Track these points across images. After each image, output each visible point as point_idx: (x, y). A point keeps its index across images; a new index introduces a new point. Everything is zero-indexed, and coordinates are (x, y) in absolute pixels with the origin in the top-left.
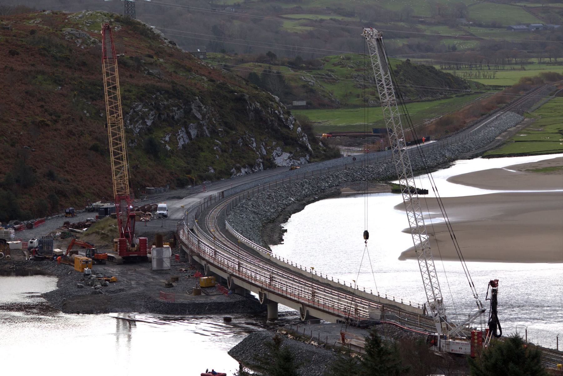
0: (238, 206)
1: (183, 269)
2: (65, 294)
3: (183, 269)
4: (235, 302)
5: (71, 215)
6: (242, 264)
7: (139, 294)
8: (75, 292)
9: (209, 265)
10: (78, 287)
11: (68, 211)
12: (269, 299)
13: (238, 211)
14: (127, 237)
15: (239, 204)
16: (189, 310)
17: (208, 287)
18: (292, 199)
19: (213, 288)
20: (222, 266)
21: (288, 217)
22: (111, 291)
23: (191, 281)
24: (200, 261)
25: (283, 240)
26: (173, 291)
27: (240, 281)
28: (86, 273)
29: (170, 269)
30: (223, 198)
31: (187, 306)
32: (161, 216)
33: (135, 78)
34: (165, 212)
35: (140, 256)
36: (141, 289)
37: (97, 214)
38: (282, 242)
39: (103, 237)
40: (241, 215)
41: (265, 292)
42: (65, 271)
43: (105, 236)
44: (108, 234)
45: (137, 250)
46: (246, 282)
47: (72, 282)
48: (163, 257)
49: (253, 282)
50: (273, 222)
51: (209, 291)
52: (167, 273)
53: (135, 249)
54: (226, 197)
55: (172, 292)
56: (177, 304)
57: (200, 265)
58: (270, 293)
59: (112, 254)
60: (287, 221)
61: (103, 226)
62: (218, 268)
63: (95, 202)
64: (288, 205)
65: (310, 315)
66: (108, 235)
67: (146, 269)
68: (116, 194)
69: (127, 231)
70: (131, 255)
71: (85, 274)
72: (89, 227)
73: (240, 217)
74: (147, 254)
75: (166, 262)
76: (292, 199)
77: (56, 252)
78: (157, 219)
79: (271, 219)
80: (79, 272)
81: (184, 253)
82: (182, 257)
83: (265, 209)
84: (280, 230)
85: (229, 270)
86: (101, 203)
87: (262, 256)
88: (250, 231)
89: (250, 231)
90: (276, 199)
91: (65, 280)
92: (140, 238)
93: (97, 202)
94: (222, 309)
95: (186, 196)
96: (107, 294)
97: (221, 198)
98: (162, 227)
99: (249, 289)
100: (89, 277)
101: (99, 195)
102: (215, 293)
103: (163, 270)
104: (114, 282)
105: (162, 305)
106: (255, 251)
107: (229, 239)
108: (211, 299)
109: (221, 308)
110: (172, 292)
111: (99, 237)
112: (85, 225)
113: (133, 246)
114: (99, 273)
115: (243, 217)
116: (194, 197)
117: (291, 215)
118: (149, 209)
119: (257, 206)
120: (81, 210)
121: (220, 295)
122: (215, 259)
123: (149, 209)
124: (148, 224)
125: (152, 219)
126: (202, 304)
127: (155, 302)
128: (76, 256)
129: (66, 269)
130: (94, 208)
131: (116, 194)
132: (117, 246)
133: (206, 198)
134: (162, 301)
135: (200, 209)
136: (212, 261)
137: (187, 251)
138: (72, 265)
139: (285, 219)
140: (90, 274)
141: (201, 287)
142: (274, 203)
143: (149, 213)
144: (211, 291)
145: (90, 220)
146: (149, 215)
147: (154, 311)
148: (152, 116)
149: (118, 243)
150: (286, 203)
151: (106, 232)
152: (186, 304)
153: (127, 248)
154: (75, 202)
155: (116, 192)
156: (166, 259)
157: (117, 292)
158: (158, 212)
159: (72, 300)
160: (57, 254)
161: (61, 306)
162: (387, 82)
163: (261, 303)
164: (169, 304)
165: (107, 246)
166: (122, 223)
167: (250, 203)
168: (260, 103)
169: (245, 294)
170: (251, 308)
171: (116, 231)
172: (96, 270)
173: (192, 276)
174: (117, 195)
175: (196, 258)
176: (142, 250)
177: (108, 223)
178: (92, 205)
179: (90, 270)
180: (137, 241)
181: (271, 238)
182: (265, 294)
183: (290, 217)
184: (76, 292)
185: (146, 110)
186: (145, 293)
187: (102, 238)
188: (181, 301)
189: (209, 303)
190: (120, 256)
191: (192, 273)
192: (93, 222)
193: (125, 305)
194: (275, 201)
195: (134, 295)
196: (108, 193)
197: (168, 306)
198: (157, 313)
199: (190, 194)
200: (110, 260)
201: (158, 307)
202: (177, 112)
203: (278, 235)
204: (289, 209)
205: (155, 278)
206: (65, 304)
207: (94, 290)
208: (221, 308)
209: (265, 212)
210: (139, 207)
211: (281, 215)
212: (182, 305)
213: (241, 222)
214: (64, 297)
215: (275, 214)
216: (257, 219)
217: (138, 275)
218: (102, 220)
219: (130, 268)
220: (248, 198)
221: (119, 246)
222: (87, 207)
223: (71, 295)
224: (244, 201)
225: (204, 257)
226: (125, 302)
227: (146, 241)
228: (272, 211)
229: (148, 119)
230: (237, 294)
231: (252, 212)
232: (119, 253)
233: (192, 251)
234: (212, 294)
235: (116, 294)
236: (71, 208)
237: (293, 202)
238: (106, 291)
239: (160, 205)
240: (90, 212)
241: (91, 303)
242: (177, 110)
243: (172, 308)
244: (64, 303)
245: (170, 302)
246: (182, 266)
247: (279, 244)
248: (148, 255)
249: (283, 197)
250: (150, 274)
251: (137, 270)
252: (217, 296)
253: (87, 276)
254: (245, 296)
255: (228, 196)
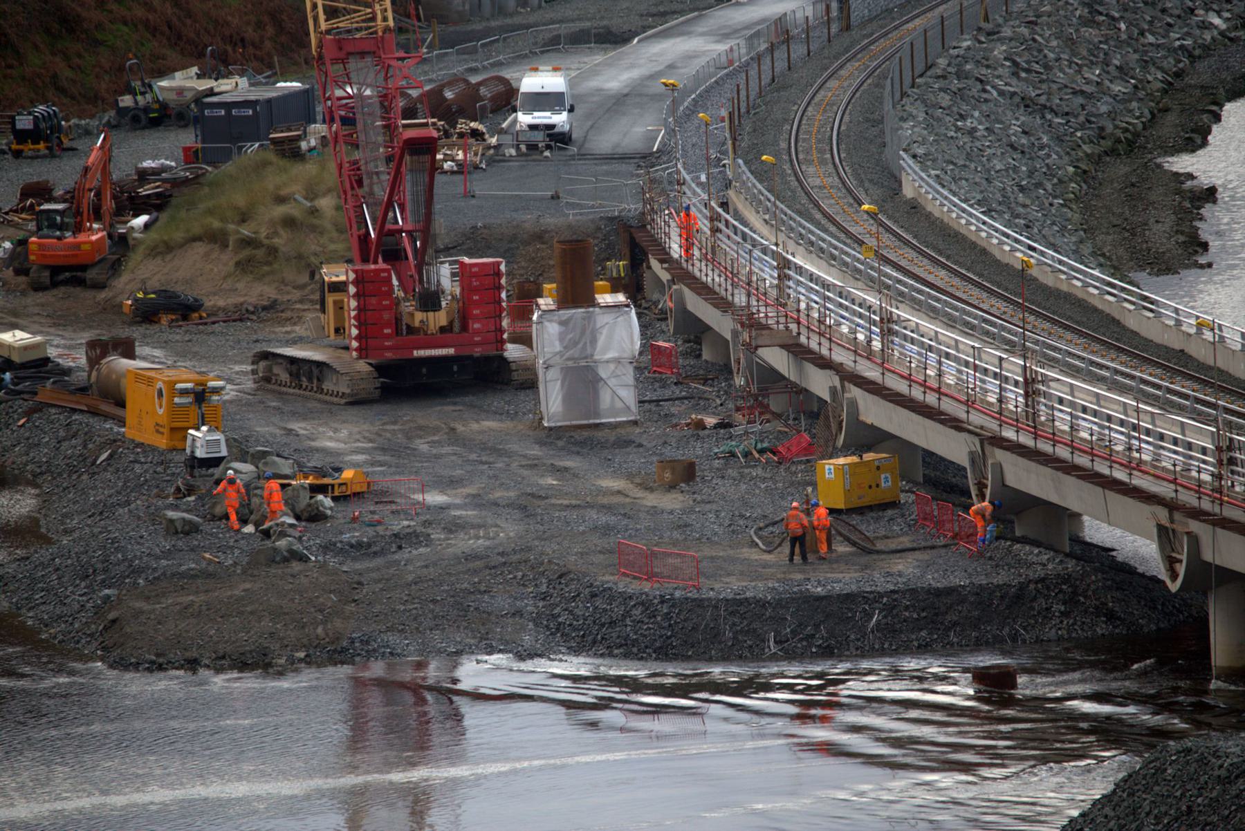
0: (939, 72)
1: (711, 421)
2: (105, 570)
3: (711, 421)
4: (1022, 587)
5: (42, 145)
6: (1045, 380)
7: (502, 554)
8: (158, 558)
9: (855, 392)
10: (172, 529)
11: (24, 122)
12: (1218, 562)
13: (945, 100)
14: (394, 255)
15: (942, 62)
16: (777, 633)
17: (860, 511)
18: (1217, 21)
19: (890, 512)
20: (931, 399)
21: (1205, 117)
22: (352, 546)
23: (764, 480)
24: (801, 370)
25: (1205, 246)
26: (676, 534)
27: (1047, 471)
28: (200, 453)
29: (635, 423)
30: (848, 28)
31: (769, 613)
32: (539, 137)
34: (560, 119)
35: (470, 357)
36: (508, 530)
37: (188, 138)
38: (1202, 260)
39: (249, 260)
40: (962, 117)
41: (1195, 526)
42: (71, 448)
43: (260, 253)
44: (276, 241)
45: (451, 323)
46: (1079, 477)
47: (128, 503)
48: (596, 357)
49: (1120, 475)
50: (1129, 153)
51: (869, 527)
52: (628, 443)
53: (440, 318)
54: (863, 25)
55: (675, 543)
56: (715, 605)
57: (800, 392)
58: (1219, 531)
59: (315, 349)
60: (1205, 143)
61: (240, 200)
63: (163, 73)
64: (1197, 52)
66: (273, 251)
67: (508, 424)
68: (324, 26)
69: (389, 226)
70: (418, 353)
71: (193, 457)
72: (159, 208)
73: (958, 129)
74: (503, 342)
75: (612, 382)
76: (1217, 21)
77: (10, 347)
78: (520, 153)
79: (1119, 133)
80: (154, 449)
81: (695, 331)
82: (685, 355)
83: (1079, 79)
84: (1179, 192)
85: (976, 419)
86: (199, 77)
87: (1136, 334)
88: (1024, 206)
89: (1024, 206)
90: (1130, 24)
91: (83, 491)
92: (466, 260)
93: (178, 74)
94: (955, 624)
95: (645, 28)
96: (332, 562)
97: (834, 28)
98: (555, 197)
99: (1073, 505)
100: (217, 472)
101: (180, 37)
102: (906, 542)
103: (597, 426)
104: (355, 494)
105: (637, 612)
106: (1095, 310)
107: (940, 253)
108: (889, 574)
109: (952, 617)
110: (675, 543)
111: (227, 260)
112: (138, 196)
113: (430, 301)
114: (265, 454)
115: (972, 131)
116: (689, 33)
117: (1221, 106)
118: (468, 106)
119: (1036, 67)
120: (92, 117)
121: (933, 547)
122: (883, 361)
123: (468, 106)
124: (480, 186)
125: (496, 158)
126: (849, 598)
127: (594, 595)
128: (125, 363)
129: (74, 436)
130: (164, 106)
131: (324, 26)
132: (339, 307)
133: (757, 35)
134: (634, 587)
135: (743, 93)
136: (871, 372)
137: (723, 324)
138: (106, 416)
139: (1193, 131)
140: (221, 459)
141: (832, 511)
142: (1120, 44)
143: (473, 125)
144: (882, 532)
145: (156, 172)
146: (475, 134)
147: (594, 642)
149: (352, 290)
150: (1188, 42)
151: (263, 233)
152: (762, 604)
153: (398, 320)
154: (55, 76)
155: (322, 17)
156: (612, 366)
157: (382, 553)
158: (525, 119)
159: (148, 598)
160: (16, 358)
161: (91, 635)
163: (1174, 587)
164: (673, 603)
165: (272, 306)
166: (360, 183)
167: (999, 51)
169: (1068, 542)
170: (1111, 616)
171: (314, 228)
172: (247, 439)
173: (761, 452)
174: (328, 32)
175: (776, 358)
176: (476, 326)
177: (271, 187)
178: (150, 87)
179: (218, 436)
180: (444, 275)
181: (1134, 235)
182: (1194, 540)
183: (1217, 118)
184: (167, 554)
186: (529, 549)
187: (244, 266)
188: (729, 586)
189: (881, 595)
190: (360, 357)
191: (762, 436)
192: (177, 183)
193: (435, 618)
194: (1124, 37)
195: (479, 564)
196: (228, 23)
197: (667, 616)
198: (611, 655)
199: (664, 16)
200: (305, 382)
201: (612, 623)
203: (1169, 221)
204: (1206, 78)
205: (566, 469)
206: (114, 621)
207: (258, 544)
208: (952, 617)
209: (1080, 100)
210: (414, 93)
211: (1166, 110)
212: (738, 606)
213: (969, 157)
214: (104, 584)
215: (1134, 104)
216: (1045, 140)
217: (473, 456)
218: (228, 167)
219: (421, 422)
220: (983, 25)
221: (358, 308)
222: (126, 101)
223: (138, 572)
224: (965, 44)
225: (825, 352)
226: (434, 601)
227: (498, 274)
228: (1117, 88)
230: (1024, 540)
231: (1017, 100)
232: (355, 344)
233: (751, 323)
234: (893, 544)
235: (379, 561)
236: (41, 108)
237: (1222, 33)
238: (327, 548)
239: (534, 82)
240: (143, 128)
241: (252, 613)
243: (689, 625)
244: (111, 616)
245: (678, 594)
246: (697, 401)
247: (1187, 267)
248: (513, 351)
249: (1164, 11)
250: (536, 451)
251: (460, 428)
252: (918, 555)
253: (204, 471)
254: (1068, 551)
255: (871, 20)
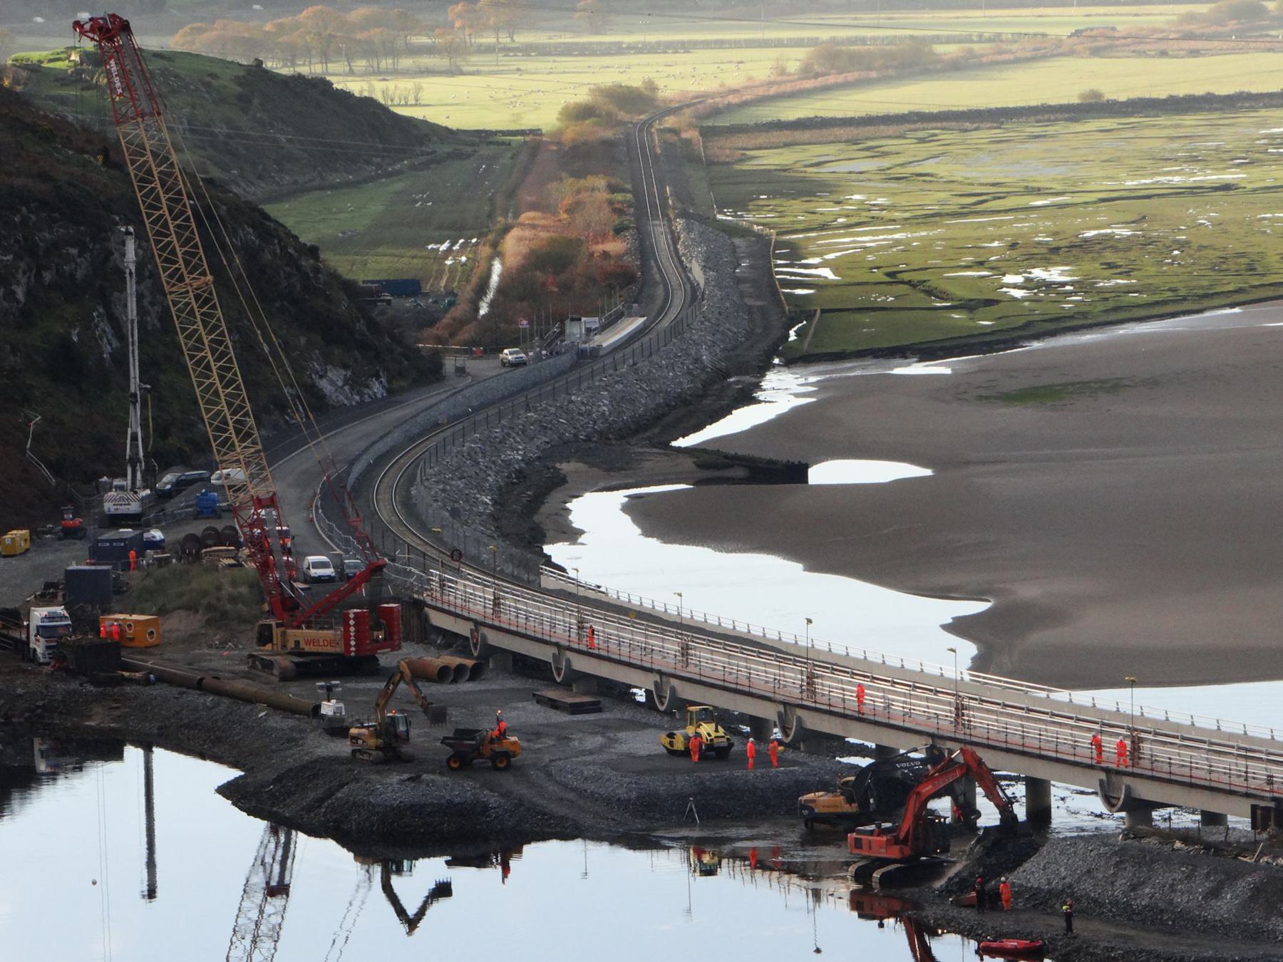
33: (53, 79)
62: (519, 636)
65: (490, 643)
148: (24, 273)
162: (190, 233)
168: (253, 227)
185: (8, 258)
202: (79, 260)
221: (355, 632)
229: (18, 283)
242: (79, 256)
